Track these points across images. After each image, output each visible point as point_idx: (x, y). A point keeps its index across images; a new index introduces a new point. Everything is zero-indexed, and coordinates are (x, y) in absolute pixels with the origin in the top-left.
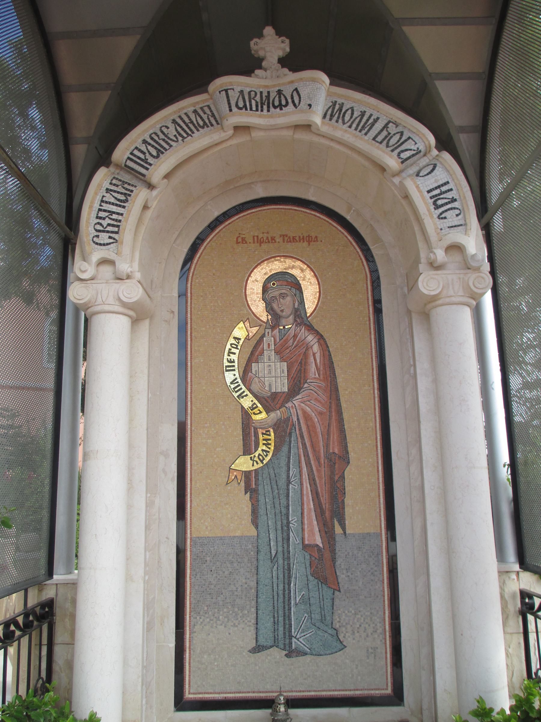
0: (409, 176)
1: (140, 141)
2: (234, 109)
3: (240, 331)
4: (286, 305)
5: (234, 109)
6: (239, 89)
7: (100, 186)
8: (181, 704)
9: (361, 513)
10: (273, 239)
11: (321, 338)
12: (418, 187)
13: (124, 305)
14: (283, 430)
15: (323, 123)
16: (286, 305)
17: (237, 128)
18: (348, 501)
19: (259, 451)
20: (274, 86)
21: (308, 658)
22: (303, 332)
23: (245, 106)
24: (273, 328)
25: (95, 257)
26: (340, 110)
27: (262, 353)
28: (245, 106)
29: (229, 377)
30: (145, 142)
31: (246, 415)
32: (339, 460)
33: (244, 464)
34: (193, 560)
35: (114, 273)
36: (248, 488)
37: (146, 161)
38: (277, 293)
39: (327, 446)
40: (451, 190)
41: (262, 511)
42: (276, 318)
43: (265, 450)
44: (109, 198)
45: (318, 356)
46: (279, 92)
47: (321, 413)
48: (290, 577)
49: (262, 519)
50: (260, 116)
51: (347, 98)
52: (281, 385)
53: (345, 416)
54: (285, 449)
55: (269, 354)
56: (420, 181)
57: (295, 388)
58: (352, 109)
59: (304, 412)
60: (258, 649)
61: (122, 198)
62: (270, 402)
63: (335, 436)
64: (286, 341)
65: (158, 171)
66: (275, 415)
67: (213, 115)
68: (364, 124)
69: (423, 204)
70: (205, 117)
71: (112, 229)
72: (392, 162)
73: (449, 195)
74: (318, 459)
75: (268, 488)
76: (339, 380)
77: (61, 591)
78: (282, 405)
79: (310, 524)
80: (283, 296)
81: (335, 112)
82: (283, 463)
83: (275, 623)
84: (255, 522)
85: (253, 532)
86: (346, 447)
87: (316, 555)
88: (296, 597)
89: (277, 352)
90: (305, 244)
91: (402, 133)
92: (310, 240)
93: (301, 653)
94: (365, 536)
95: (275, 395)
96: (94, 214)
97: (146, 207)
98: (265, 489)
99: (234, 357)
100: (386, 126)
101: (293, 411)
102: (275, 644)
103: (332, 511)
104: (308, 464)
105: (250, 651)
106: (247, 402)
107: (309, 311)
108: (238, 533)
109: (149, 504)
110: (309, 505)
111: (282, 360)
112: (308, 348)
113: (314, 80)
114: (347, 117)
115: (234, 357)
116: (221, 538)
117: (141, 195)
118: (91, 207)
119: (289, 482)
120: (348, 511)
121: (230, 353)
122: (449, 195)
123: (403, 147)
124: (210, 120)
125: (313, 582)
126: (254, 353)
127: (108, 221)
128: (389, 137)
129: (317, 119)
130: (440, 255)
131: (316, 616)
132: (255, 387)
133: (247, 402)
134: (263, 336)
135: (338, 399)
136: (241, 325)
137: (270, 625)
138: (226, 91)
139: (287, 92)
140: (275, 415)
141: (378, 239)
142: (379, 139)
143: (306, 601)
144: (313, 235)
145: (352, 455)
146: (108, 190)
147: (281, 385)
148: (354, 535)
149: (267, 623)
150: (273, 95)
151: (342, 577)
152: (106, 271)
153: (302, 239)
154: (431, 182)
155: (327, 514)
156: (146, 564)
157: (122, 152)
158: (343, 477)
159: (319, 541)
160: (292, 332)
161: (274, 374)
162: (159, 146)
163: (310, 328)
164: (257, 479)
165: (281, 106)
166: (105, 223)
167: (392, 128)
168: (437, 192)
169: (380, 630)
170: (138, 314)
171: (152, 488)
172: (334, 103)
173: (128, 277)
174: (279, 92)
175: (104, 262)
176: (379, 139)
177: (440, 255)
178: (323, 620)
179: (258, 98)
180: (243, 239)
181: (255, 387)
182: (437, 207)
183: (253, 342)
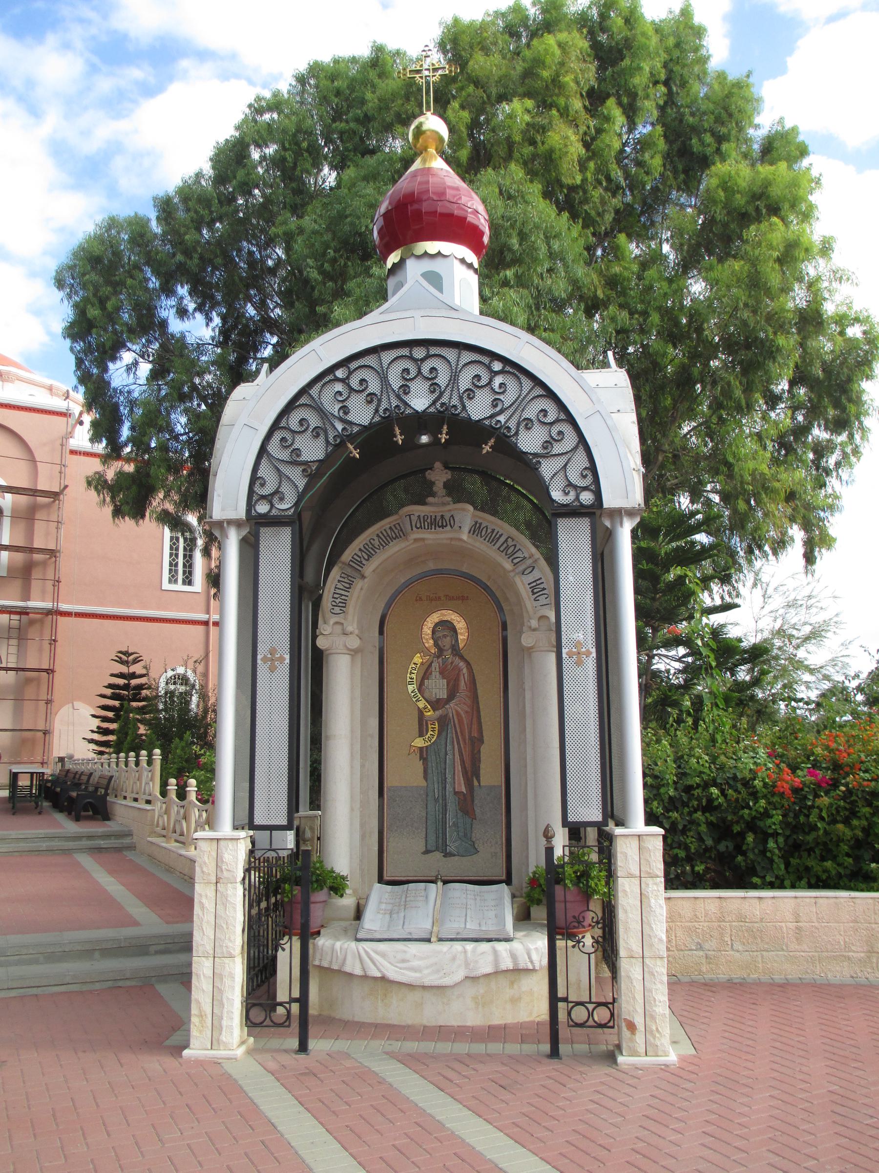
0: (518, 574)
1: (357, 549)
2: (414, 529)
3: (418, 659)
4: (447, 642)
5: (414, 529)
6: (417, 514)
7: (334, 578)
8: (381, 880)
9: (490, 774)
10: (440, 598)
11: (468, 664)
12: (522, 581)
13: (348, 649)
14: (443, 722)
15: (469, 537)
16: (447, 642)
17: (416, 540)
18: (482, 766)
19: (429, 735)
20: (439, 512)
21: (456, 858)
22: (457, 660)
23: (421, 526)
24: (438, 657)
25: (332, 622)
26: (479, 527)
27: (431, 674)
28: (421, 526)
29: (410, 688)
30: (360, 550)
31: (421, 712)
32: (477, 741)
33: (419, 743)
34: (388, 800)
35: (343, 630)
36: (421, 757)
37: (361, 562)
38: (441, 635)
39: (470, 733)
41: (430, 771)
42: (441, 651)
43: (432, 734)
44: (340, 586)
45: (466, 675)
46: (442, 516)
47: (467, 712)
48: (446, 810)
49: (430, 776)
50: (430, 533)
51: (484, 519)
52: (443, 695)
53: (482, 713)
54: (444, 734)
55: (435, 674)
56: (524, 577)
57: (451, 696)
58: (487, 527)
59: (457, 711)
60: (427, 852)
61: (348, 586)
62: (436, 704)
63: (475, 726)
64: (446, 666)
65: (369, 569)
66: (439, 713)
67: (402, 530)
68: (493, 538)
69: (524, 591)
70: (396, 531)
71: (342, 605)
72: (508, 566)
73: (542, 586)
74: (464, 740)
75: (433, 757)
76: (479, 691)
77: (303, 821)
78: (443, 707)
79: (459, 779)
80: (445, 636)
81: (476, 529)
82: (443, 742)
83: (437, 837)
84: (426, 777)
85: (424, 784)
86: (482, 733)
87: (462, 797)
88: (450, 822)
89: (440, 673)
90: (460, 602)
91: (515, 546)
92: (463, 598)
93: (451, 855)
94: (492, 788)
95: (438, 700)
96: (331, 596)
97: (361, 589)
99: (414, 676)
100: (506, 541)
101: (450, 710)
102: (437, 849)
103: (472, 772)
104: (458, 743)
106: (422, 704)
107: (461, 645)
108: (415, 784)
109: (362, 766)
110: (459, 768)
111: (444, 678)
112: (460, 670)
113: (464, 510)
114: (483, 533)
115: (414, 676)
116: (405, 787)
117: (359, 584)
118: (329, 591)
119: (446, 754)
120: (482, 772)
121: (411, 673)
122: (542, 586)
123: (515, 556)
124: (398, 533)
125: (460, 814)
126: (426, 675)
127: (339, 600)
128: (507, 548)
129: (465, 537)
130: (534, 623)
131: (461, 834)
132: (427, 695)
133: (422, 704)
134: (432, 662)
135: (478, 703)
136: (418, 655)
137: (434, 838)
138: (410, 515)
139: (447, 517)
140: (439, 713)
141: (507, 599)
142: (502, 549)
143: (455, 825)
144: (466, 595)
145: (485, 738)
146: (339, 581)
147: (443, 695)
148: (485, 786)
149: (432, 838)
150: (438, 518)
151: (478, 811)
152: (338, 628)
153: (458, 598)
154: (530, 578)
155: (469, 774)
156: (361, 802)
157: (347, 556)
158: (479, 751)
159: (464, 790)
160: (450, 660)
161: (438, 687)
162: (369, 552)
163: (462, 658)
164: (427, 752)
165: (443, 527)
166: (337, 601)
167: (510, 542)
168: (534, 584)
169: (499, 843)
170: (354, 653)
171: (364, 757)
172: (476, 523)
173: (351, 633)
174: (442, 516)
175: (337, 623)
176: (502, 549)
177: (534, 623)
178: (465, 835)
179: (429, 520)
180: (420, 598)
181: (427, 695)
182: (534, 593)
183: (425, 667)
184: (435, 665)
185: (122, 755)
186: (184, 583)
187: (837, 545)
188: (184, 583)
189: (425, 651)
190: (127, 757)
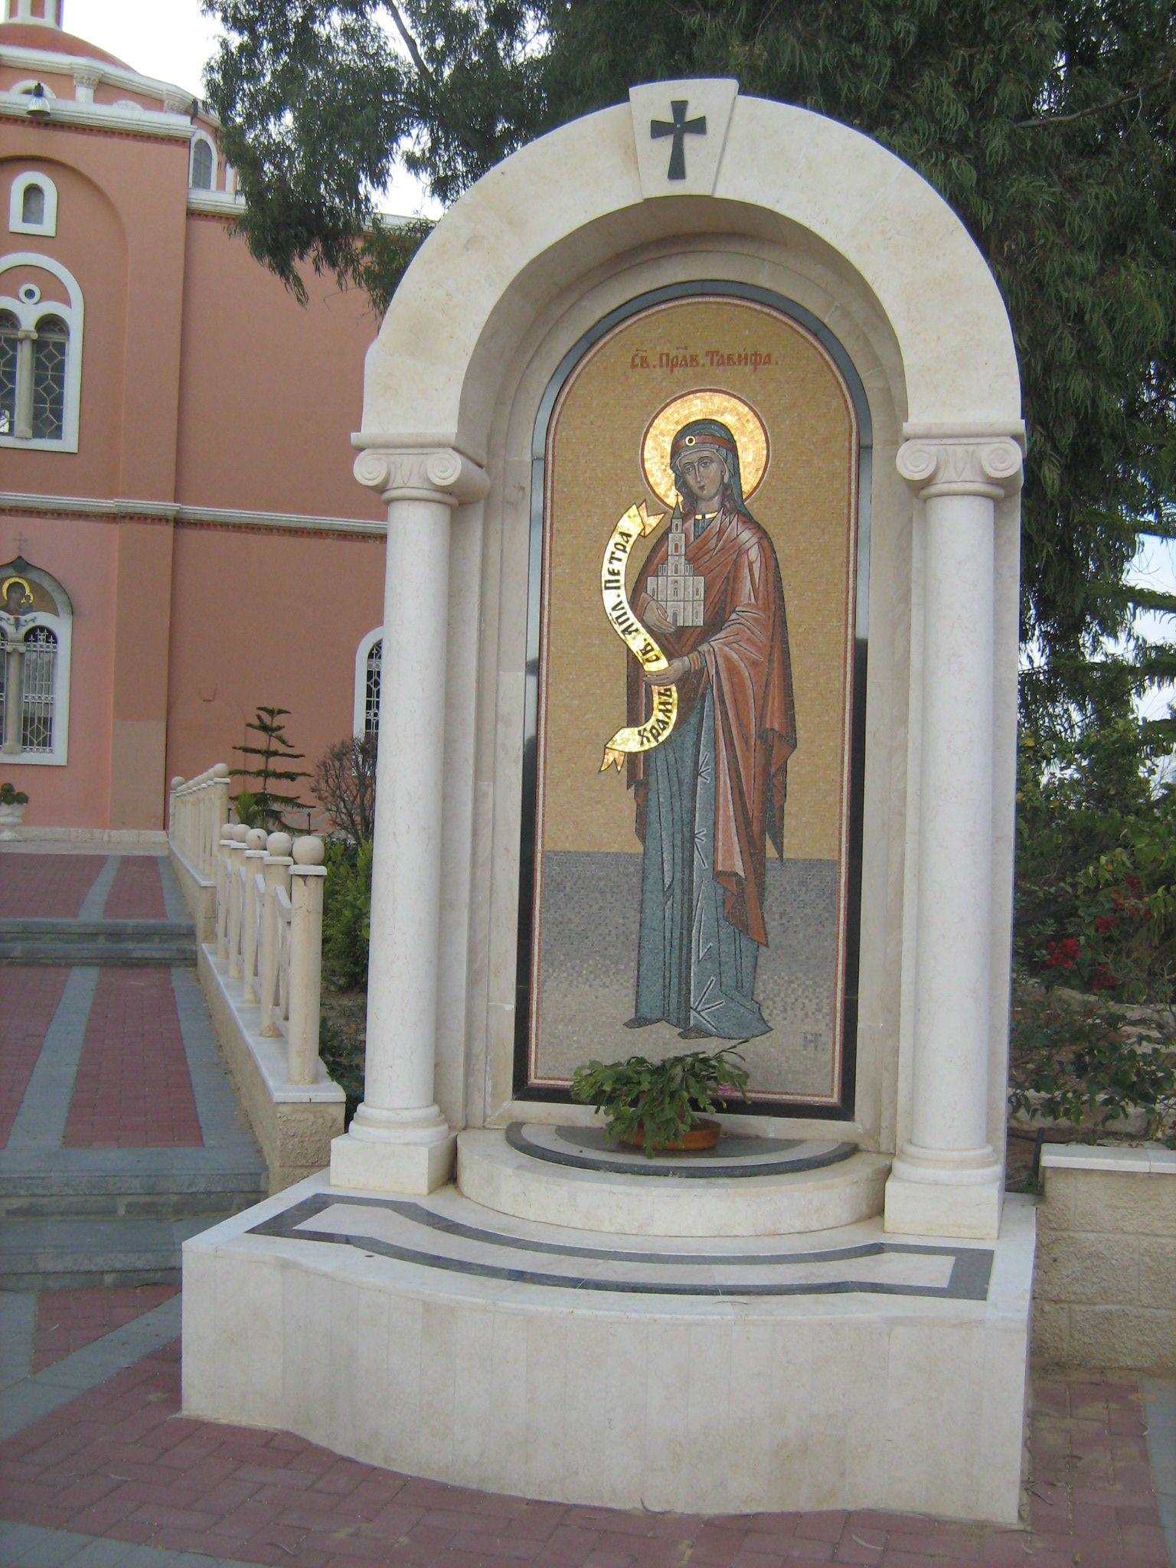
14: (692, 689)
31: (634, 665)
43: (665, 713)
52: (694, 615)
55: (676, 561)
62: (672, 642)
88: (699, 950)
92: (757, 360)
98: (661, 785)
126: (650, 559)
147: (694, 615)
161: (683, 596)
184: (676, 538)
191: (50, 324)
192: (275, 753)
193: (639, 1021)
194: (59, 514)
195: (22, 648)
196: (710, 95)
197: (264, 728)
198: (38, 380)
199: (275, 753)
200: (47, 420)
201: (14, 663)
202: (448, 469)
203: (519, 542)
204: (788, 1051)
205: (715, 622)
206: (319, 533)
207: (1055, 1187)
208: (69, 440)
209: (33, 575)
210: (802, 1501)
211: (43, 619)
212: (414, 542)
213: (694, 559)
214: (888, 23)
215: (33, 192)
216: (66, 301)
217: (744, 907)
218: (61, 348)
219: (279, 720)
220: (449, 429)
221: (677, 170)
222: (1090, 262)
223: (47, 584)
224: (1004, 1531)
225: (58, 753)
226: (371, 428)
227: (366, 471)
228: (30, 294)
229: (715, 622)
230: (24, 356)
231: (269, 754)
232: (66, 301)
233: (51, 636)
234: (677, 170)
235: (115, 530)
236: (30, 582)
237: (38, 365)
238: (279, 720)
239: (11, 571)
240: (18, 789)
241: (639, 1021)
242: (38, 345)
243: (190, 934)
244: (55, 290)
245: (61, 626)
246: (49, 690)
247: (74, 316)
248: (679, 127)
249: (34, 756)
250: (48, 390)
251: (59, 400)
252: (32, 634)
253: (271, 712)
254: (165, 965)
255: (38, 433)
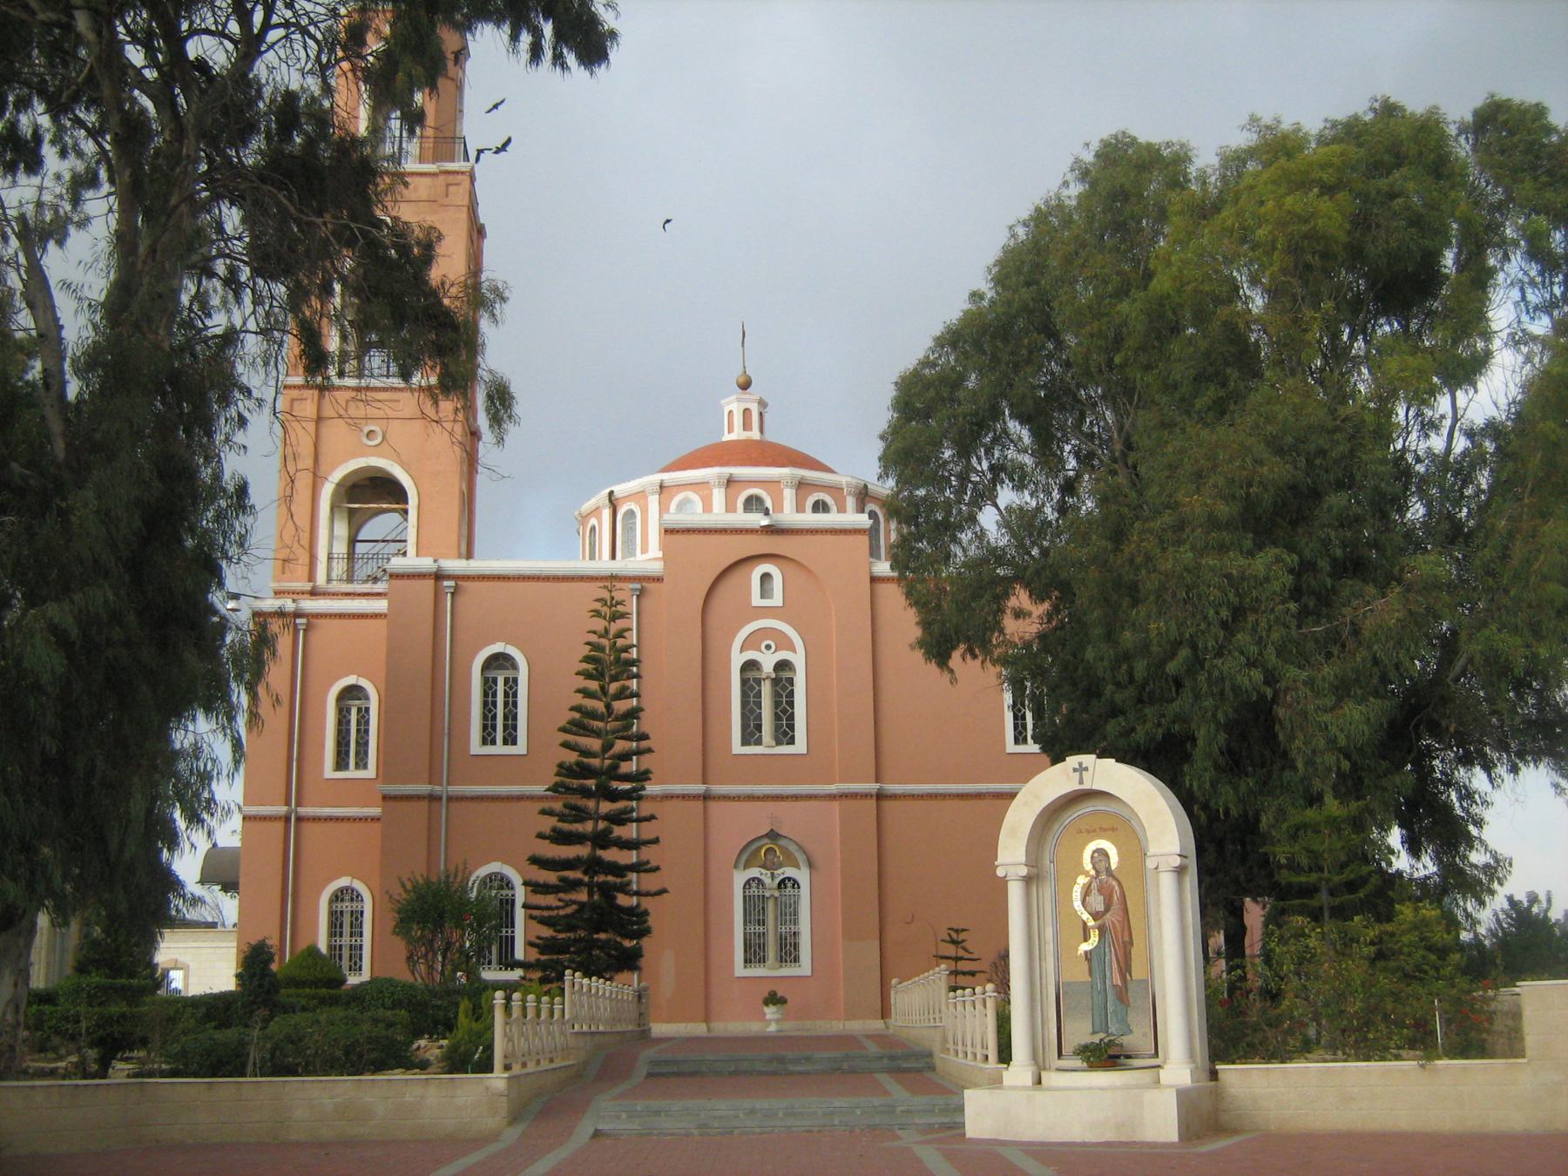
14: (1102, 930)
31: (1085, 924)
40: (613, 557)
43: (1094, 938)
52: (1101, 908)
55: (1095, 892)
62: (1096, 916)
88: (1110, 1008)
92: (1113, 829)
98: (1095, 959)
105: (880, 477)
110: (1115, 966)
126: (1087, 892)
147: (1101, 908)
149: (1097, 1022)
161: (1097, 902)
184: (1094, 885)
185: (531, 997)
186: (505, 742)
187: (601, 71)
188: (505, 742)
189: (1087, 874)
190: (524, 1001)
191: (783, 666)
192: (961, 959)
193: (1094, 1033)
194: (796, 798)
195: (777, 894)
196: (1088, 759)
197: (953, 942)
198: (777, 704)
199: (961, 959)
200: (785, 734)
201: (770, 906)
202: (1024, 871)
203: (1047, 891)
204: (1137, 1038)
205: (1107, 909)
206: (979, 796)
207: (1221, 1075)
208: (800, 746)
209: (783, 842)
210: (1124, 1139)
211: (789, 872)
212: (1015, 893)
213: (1100, 891)
214: (1217, 613)
215: (766, 577)
216: (793, 649)
217: (1122, 995)
218: (791, 681)
219: (962, 936)
220: (1023, 859)
221: (1081, 782)
222: (1329, 701)
223: (792, 848)
224: (1172, 1145)
225: (805, 967)
226: (1000, 860)
227: (1000, 872)
228: (768, 647)
229: (1107, 909)
230: (766, 689)
231: (957, 959)
232: (793, 649)
233: (796, 884)
234: (1081, 782)
235: (836, 804)
236: (780, 847)
237: (776, 696)
238: (962, 936)
239: (766, 840)
240: (780, 994)
241: (1094, 1033)
242: (776, 682)
243: (930, 1055)
244: (784, 643)
245: (802, 875)
246: (796, 922)
247: (798, 659)
248: (1081, 769)
249: (788, 971)
250: (785, 711)
251: (791, 717)
252: (782, 884)
253: (957, 931)
254: (920, 1071)
255: (779, 743)
